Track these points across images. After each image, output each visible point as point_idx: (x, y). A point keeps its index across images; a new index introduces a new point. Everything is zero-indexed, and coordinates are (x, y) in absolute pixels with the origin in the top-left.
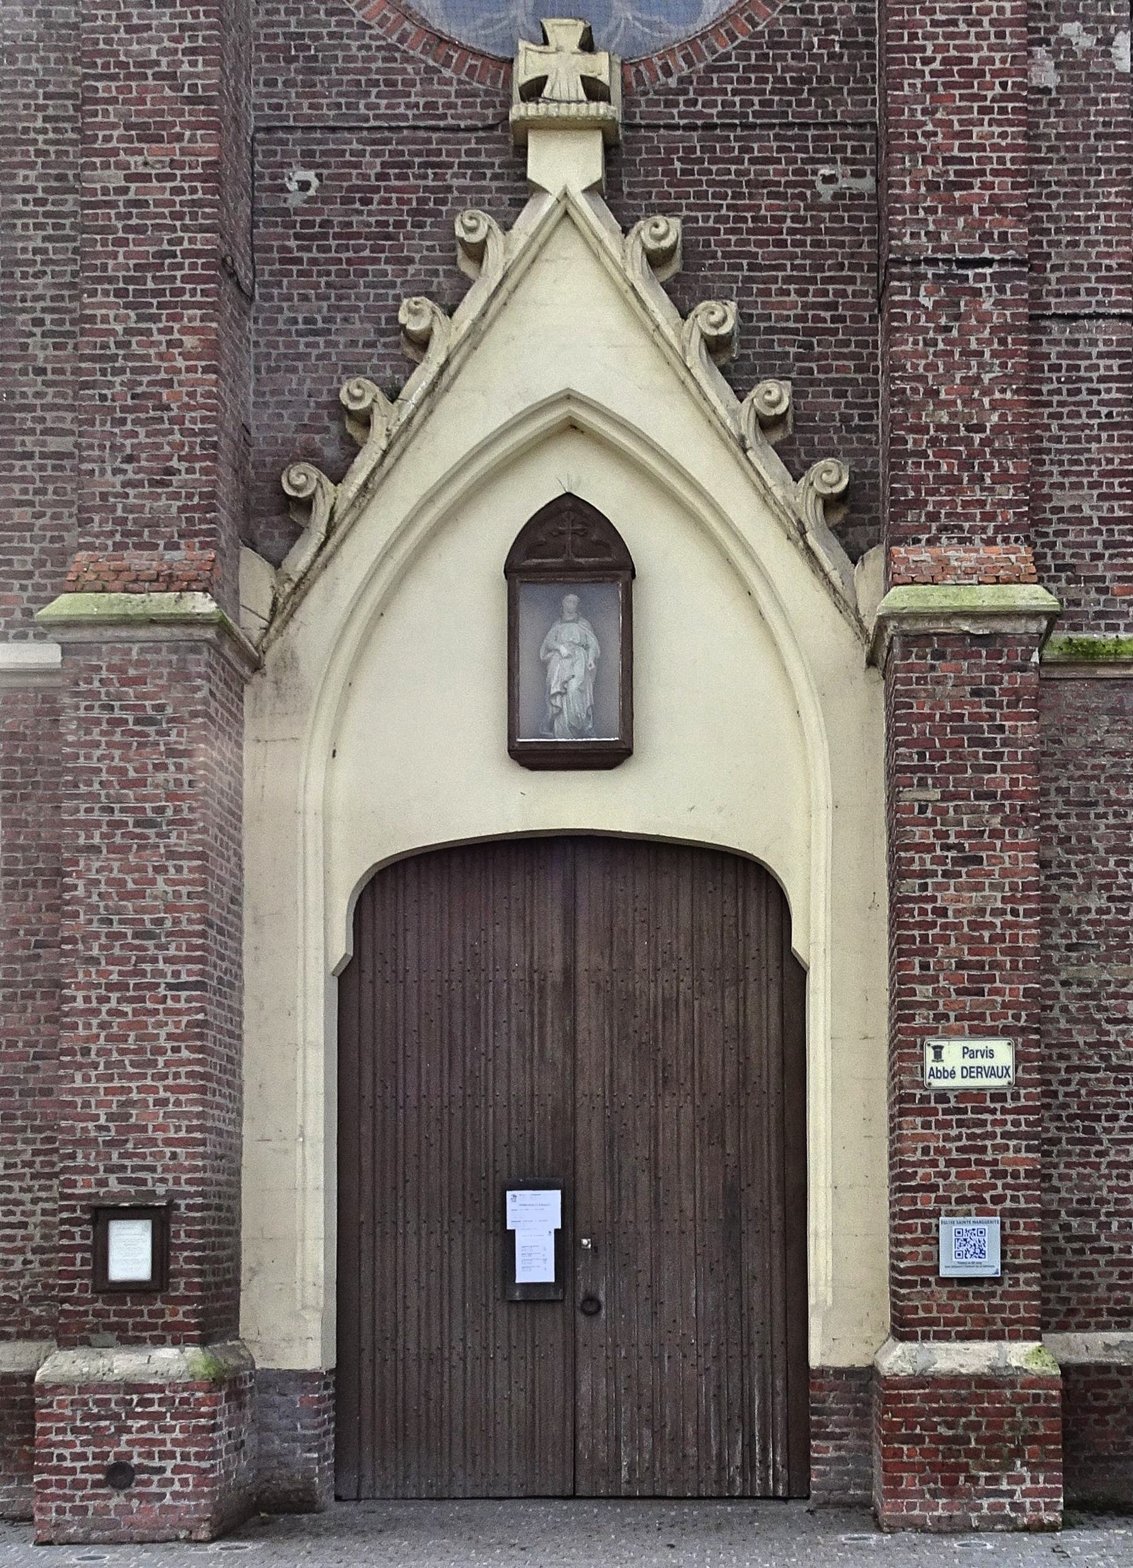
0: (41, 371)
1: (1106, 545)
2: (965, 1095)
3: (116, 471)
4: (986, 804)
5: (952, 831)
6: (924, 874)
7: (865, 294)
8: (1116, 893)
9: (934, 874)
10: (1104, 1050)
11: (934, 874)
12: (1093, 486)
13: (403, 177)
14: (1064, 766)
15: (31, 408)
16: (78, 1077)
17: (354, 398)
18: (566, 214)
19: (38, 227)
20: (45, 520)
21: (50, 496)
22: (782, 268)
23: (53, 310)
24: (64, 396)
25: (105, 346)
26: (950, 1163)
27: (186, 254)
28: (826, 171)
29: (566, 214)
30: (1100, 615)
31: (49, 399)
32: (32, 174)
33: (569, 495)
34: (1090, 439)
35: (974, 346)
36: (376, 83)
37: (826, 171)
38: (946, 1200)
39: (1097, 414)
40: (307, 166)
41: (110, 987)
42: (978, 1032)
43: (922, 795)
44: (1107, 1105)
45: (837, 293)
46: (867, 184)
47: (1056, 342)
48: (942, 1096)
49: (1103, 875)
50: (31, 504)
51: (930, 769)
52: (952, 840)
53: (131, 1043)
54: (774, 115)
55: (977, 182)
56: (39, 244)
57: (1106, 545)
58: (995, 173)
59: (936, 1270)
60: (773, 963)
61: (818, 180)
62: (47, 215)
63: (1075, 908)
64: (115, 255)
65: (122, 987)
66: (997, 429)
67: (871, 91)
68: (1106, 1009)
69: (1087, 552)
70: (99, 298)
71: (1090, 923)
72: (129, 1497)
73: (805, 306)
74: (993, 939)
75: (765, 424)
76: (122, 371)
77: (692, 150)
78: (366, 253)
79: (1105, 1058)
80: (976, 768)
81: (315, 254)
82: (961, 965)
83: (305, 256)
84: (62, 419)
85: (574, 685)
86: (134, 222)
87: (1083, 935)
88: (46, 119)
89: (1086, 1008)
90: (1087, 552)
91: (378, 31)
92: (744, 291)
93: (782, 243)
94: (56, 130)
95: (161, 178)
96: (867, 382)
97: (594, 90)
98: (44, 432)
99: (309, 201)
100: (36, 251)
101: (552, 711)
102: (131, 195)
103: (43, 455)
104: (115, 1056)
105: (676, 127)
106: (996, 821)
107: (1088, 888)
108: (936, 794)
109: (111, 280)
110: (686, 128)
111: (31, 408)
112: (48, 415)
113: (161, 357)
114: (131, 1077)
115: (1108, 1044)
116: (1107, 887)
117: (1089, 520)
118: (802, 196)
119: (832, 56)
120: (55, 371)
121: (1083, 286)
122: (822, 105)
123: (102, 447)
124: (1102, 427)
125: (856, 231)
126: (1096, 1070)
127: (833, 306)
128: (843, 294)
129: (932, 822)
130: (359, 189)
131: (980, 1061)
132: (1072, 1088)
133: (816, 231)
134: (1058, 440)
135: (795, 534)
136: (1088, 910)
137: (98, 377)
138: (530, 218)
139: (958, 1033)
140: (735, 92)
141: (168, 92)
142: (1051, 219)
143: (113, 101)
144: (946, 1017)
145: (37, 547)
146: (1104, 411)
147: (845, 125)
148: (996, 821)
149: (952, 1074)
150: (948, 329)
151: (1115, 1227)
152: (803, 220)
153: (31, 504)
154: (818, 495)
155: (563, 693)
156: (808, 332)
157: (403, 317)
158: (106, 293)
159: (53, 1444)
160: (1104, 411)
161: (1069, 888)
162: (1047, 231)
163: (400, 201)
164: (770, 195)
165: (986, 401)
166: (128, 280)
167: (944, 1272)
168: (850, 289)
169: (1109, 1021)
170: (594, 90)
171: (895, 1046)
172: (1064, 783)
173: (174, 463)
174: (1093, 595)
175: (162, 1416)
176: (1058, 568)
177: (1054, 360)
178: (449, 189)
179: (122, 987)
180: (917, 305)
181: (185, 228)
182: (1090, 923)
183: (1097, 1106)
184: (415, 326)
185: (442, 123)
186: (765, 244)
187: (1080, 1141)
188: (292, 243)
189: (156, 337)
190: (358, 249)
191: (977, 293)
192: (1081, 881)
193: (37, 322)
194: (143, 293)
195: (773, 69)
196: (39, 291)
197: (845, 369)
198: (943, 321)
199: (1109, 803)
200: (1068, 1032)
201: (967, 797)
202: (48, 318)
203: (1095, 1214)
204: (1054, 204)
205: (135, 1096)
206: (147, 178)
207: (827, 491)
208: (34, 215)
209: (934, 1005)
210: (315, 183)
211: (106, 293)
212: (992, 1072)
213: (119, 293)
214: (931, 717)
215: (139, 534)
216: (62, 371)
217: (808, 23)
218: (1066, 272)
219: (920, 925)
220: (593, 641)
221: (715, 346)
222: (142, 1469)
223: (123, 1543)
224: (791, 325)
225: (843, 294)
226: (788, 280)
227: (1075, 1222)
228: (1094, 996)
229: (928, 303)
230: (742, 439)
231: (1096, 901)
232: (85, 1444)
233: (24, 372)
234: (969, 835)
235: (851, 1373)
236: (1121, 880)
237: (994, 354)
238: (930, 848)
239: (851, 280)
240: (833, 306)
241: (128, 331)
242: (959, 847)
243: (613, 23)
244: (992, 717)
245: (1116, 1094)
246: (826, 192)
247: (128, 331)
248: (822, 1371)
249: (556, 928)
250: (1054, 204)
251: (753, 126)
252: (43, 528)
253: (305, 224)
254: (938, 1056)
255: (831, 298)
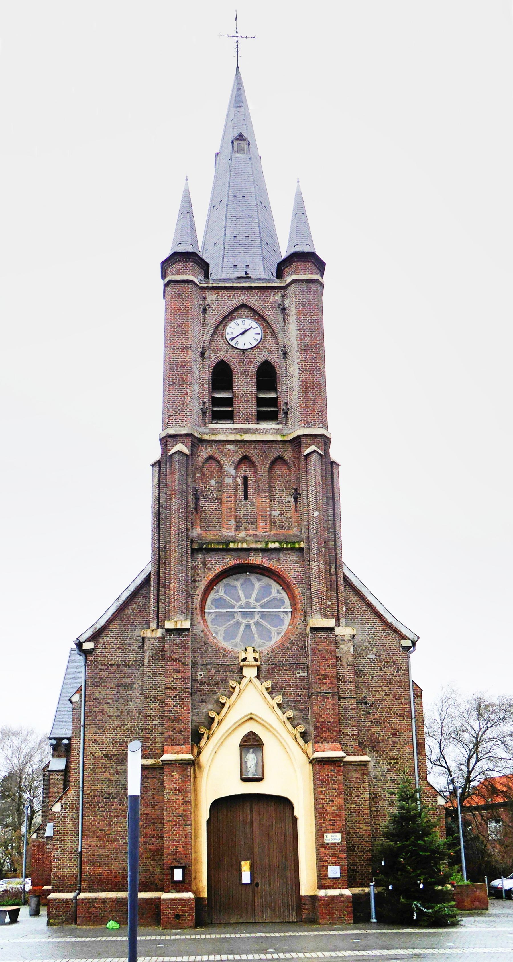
0: (152, 709)
1: (353, 740)
2: (332, 844)
3: (172, 731)
4: (334, 791)
5: (328, 796)
6: (323, 803)
7: (306, 694)
8: (357, 804)
9: (325, 803)
10: (356, 834)
11: (325, 803)
12: (350, 728)
13: (219, 673)
14: (346, 780)
15: (150, 716)
16: (168, 842)
17: (212, 715)
18: (250, 681)
19: (151, 683)
20: (153, 737)
21: (153, 732)
22: (290, 689)
23: (154, 698)
24: (156, 714)
25: (170, 709)
26: (330, 856)
27: (184, 692)
28: (298, 672)
29: (250, 681)
30: (352, 752)
31: (153, 714)
32: (150, 673)
33: (251, 732)
34: (349, 720)
35: (328, 707)
36: (214, 656)
37: (298, 672)
38: (329, 863)
39: (350, 716)
40: (201, 672)
41: (174, 826)
42: (334, 832)
43: (322, 789)
44: (357, 844)
45: (301, 694)
46: (306, 674)
47: (342, 702)
48: (328, 844)
49: (354, 801)
50: (150, 733)
51: (324, 785)
52: (328, 797)
53: (177, 836)
54: (288, 662)
55: (328, 678)
56: (151, 686)
57: (353, 740)
58: (331, 677)
59: (328, 876)
60: (291, 818)
61: (296, 673)
62: (153, 681)
63: (349, 807)
64: (171, 693)
65: (175, 825)
66: (333, 722)
67: (306, 657)
68: (356, 826)
69: (349, 741)
70: (168, 700)
71: (353, 810)
72: (179, 920)
73: (295, 696)
74: (336, 815)
75: (288, 719)
76: (173, 713)
77: (273, 668)
78: (212, 687)
79: (356, 835)
80: (332, 785)
81: (203, 687)
82: (330, 820)
83: (201, 688)
84: (156, 718)
85: (252, 766)
86: (175, 687)
87: (351, 812)
88: (153, 663)
89: (352, 826)
90: (349, 741)
91: (214, 647)
92: (283, 694)
93: (290, 685)
94: (154, 665)
95: (180, 679)
96: (307, 710)
97: (256, 659)
98: (152, 720)
99: (202, 678)
100: (151, 687)
101: (248, 771)
102: (174, 682)
103: (152, 725)
104: (174, 838)
105: (270, 664)
106: (336, 794)
107: (352, 803)
108: (325, 789)
109: (171, 697)
110: (272, 664)
111: (150, 716)
112: (153, 717)
113: (180, 710)
114: (177, 842)
115: (357, 833)
116: (356, 803)
117: (349, 735)
118: (294, 676)
119: (298, 651)
120: (154, 709)
121: (346, 692)
122: (297, 660)
123: (169, 727)
124: (351, 718)
125: (304, 683)
126: (355, 838)
127: (300, 696)
128: (302, 694)
129: (324, 794)
130: (211, 675)
131: (334, 838)
132: (350, 841)
133: (296, 683)
134: (343, 720)
135: (294, 739)
136: (352, 807)
137: (168, 714)
138: (245, 681)
139: (331, 833)
140: (281, 658)
141: (181, 664)
142: (340, 680)
143: (171, 665)
144: (328, 830)
145: (151, 742)
146: (351, 715)
147: (301, 663)
148: (336, 794)
149: (329, 840)
150: (323, 705)
151: (360, 868)
152: (294, 681)
153: (150, 733)
154: (299, 732)
155: (250, 767)
156: (296, 701)
157: (220, 700)
158: (170, 699)
159: (164, 910)
160: (351, 715)
161: (348, 803)
162: (339, 682)
163: (219, 678)
164: (288, 676)
165: (331, 717)
166: (174, 697)
167: (329, 877)
168: (303, 693)
169: (357, 828)
170: (256, 659)
171: (317, 834)
172: (346, 784)
173: (182, 730)
174: (351, 748)
175: (185, 905)
176: (344, 744)
177: (341, 706)
178: (228, 676)
179: (175, 825)
180: (318, 700)
181: (184, 688)
182: (353, 810)
183: (355, 844)
184: (223, 701)
185: (226, 664)
186: (287, 685)
187: (352, 851)
188: (199, 685)
189: (179, 707)
190: (211, 686)
191: (328, 698)
192: (350, 802)
193: (151, 700)
194: (177, 699)
195: (288, 654)
196: (152, 694)
197: (303, 708)
198: (322, 703)
199: (355, 787)
200: (349, 831)
201: (330, 790)
202: (153, 699)
203: (356, 865)
204: (340, 677)
205: (178, 845)
206: (177, 679)
207: (301, 731)
208: (150, 681)
209: (325, 827)
210: (203, 675)
211: (170, 699)
212: (337, 840)
213: (173, 699)
214: (323, 775)
215: (176, 742)
216: (156, 709)
217: (294, 645)
218: (343, 690)
219: (323, 813)
220: (255, 758)
221: (279, 705)
222: (181, 915)
223: (186, 928)
224: (292, 700)
225: (302, 694)
226: (291, 692)
227: (352, 867)
228: (354, 823)
229: (319, 700)
230: (284, 722)
231: (353, 806)
232: (171, 910)
233: (149, 709)
234: (331, 796)
235: (310, 897)
236: (358, 802)
237: (332, 709)
238: (324, 799)
239: (303, 692)
240: (300, 696)
241: (174, 706)
242: (329, 799)
243: (255, 642)
244: (334, 775)
245: (359, 842)
246: (298, 676)
247: (174, 706)
248: (304, 896)
249: (249, 812)
250: (340, 677)
251: (284, 664)
252: (152, 738)
253: (201, 682)
254: (327, 837)
255: (300, 695)
